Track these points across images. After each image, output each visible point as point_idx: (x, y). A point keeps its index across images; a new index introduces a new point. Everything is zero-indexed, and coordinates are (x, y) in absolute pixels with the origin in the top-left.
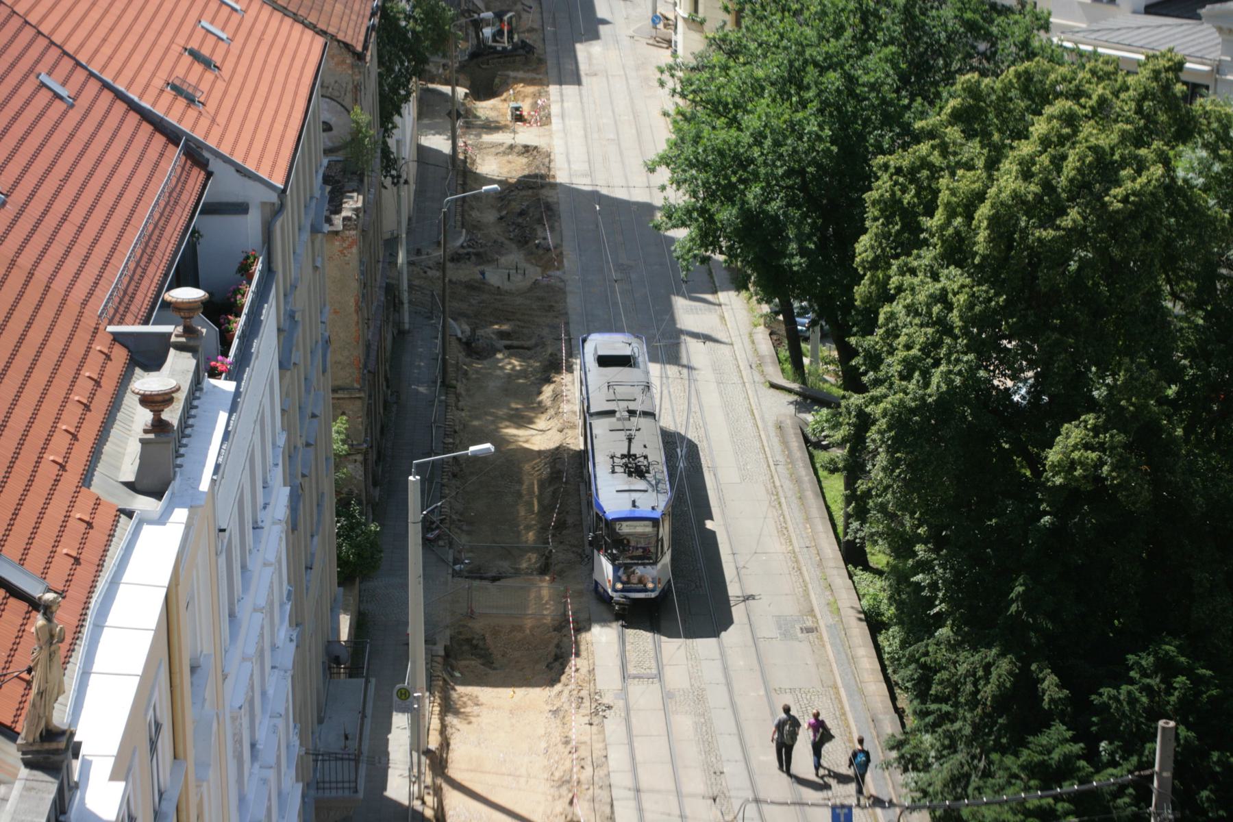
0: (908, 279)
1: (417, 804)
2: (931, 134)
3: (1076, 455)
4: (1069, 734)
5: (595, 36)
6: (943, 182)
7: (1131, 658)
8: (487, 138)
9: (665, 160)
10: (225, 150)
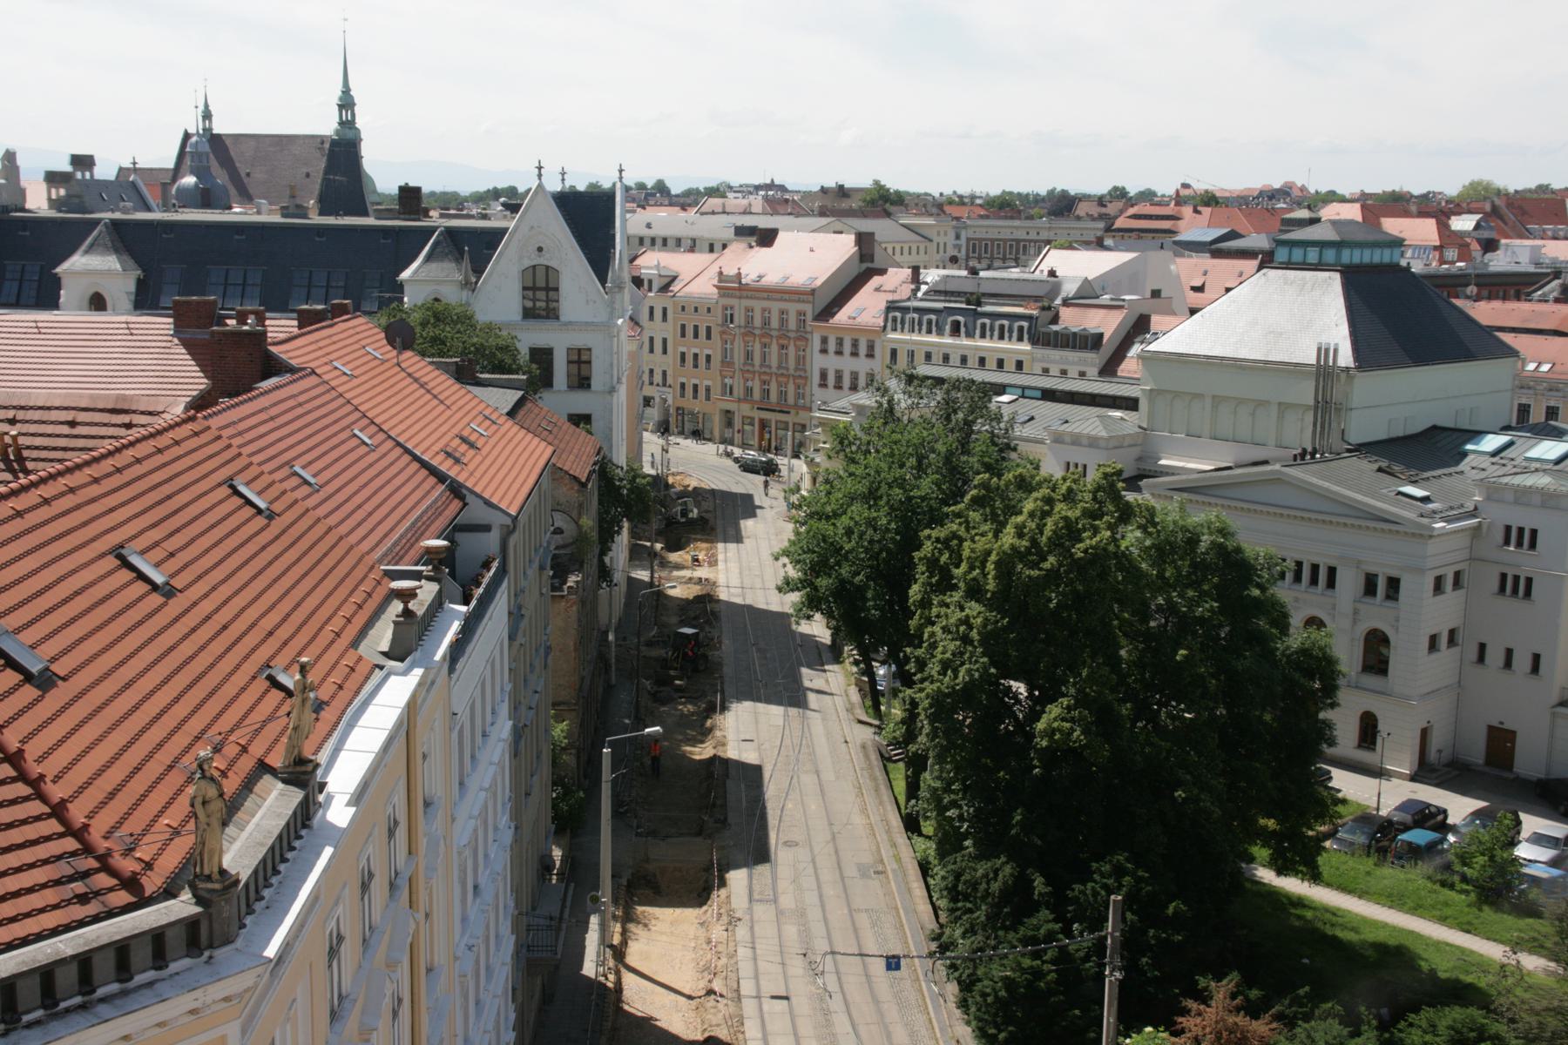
0: (943, 610)
1: (602, 979)
2: (958, 515)
3: (1055, 725)
4: (1051, 917)
5: (754, 515)
6: (966, 544)
7: (1095, 865)
8: (676, 573)
9: (786, 553)
10: (478, 490)
